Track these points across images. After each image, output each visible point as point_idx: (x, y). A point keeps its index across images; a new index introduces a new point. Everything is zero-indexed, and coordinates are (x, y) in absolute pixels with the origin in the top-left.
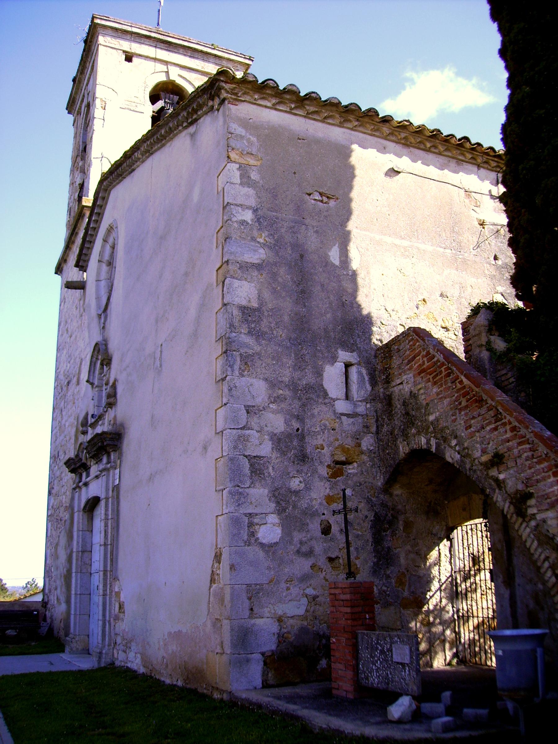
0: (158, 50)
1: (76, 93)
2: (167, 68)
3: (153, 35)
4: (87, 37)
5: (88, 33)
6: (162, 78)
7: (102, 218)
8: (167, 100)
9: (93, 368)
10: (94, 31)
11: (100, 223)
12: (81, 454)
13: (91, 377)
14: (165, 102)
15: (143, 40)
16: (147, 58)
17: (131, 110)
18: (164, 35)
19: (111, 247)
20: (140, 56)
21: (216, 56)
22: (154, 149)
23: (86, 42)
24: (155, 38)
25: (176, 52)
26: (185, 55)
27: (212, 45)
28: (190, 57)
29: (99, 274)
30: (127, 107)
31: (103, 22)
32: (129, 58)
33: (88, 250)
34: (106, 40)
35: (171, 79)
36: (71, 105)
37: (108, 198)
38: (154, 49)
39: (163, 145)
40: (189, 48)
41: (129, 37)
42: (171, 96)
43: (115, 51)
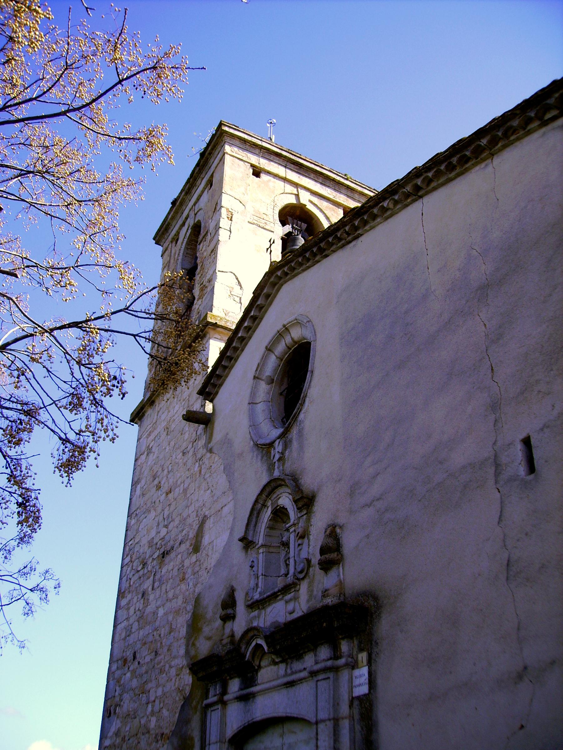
0: (288, 170)
1: (173, 218)
2: (298, 191)
3: (284, 153)
4: (206, 149)
5: (208, 145)
6: (292, 200)
7: (258, 324)
8: (294, 226)
9: (254, 520)
10: (219, 138)
11: (254, 331)
12: (243, 647)
13: (251, 533)
14: (293, 227)
15: (272, 157)
16: (276, 176)
17: (260, 226)
18: (295, 156)
19: (277, 357)
20: (268, 173)
21: (348, 187)
22: (430, 188)
23: (202, 155)
24: (285, 157)
25: (306, 177)
26: (316, 181)
27: (345, 175)
28: (321, 183)
29: (254, 394)
30: (256, 222)
31: (232, 131)
32: (257, 172)
33: (224, 371)
34: (233, 150)
35: (301, 202)
36: (163, 234)
37: (275, 297)
38: (283, 169)
39: (467, 170)
40: (321, 174)
41: (257, 151)
42: (299, 222)
43: (242, 163)
